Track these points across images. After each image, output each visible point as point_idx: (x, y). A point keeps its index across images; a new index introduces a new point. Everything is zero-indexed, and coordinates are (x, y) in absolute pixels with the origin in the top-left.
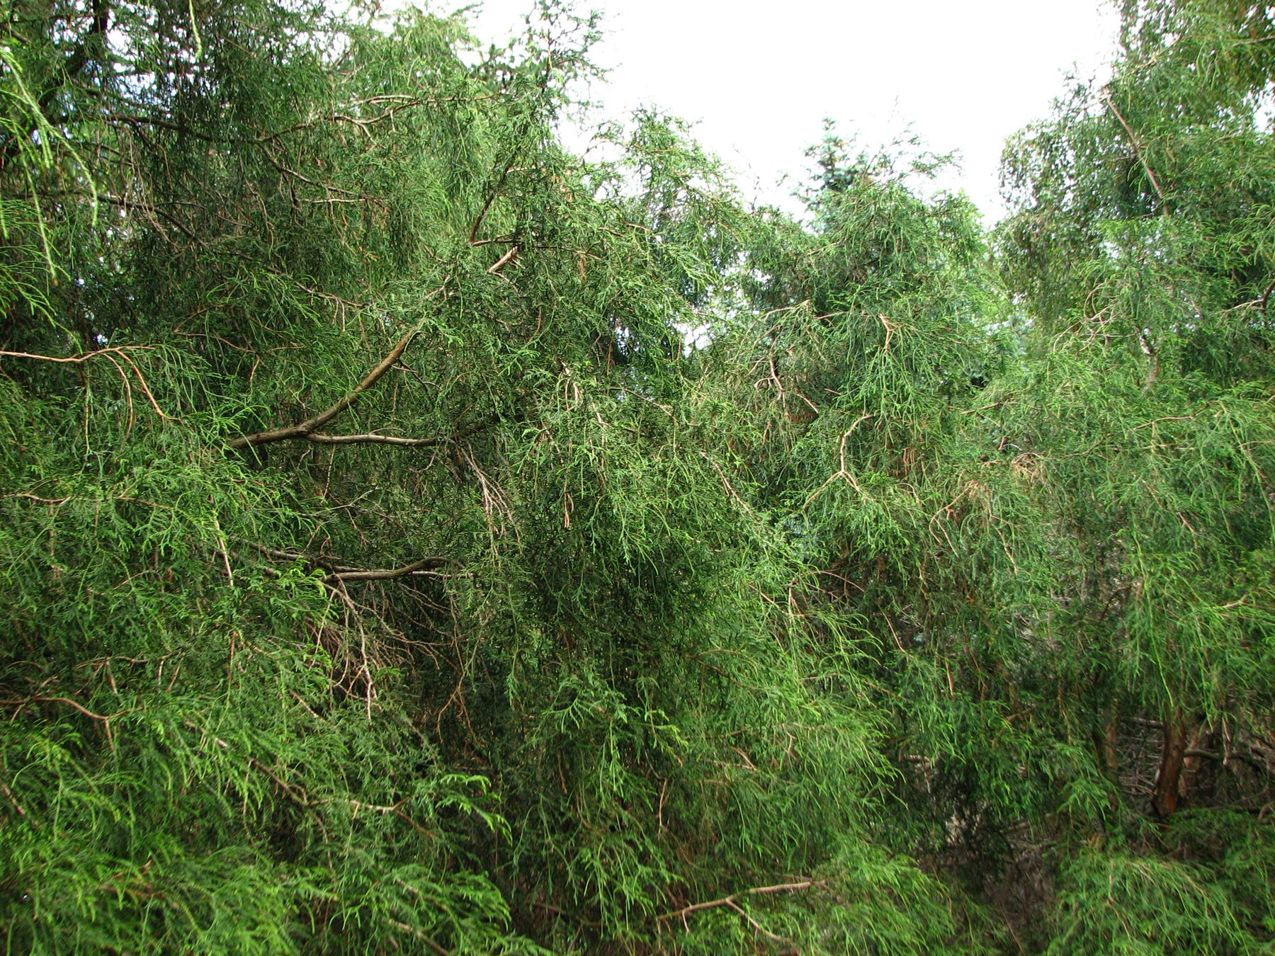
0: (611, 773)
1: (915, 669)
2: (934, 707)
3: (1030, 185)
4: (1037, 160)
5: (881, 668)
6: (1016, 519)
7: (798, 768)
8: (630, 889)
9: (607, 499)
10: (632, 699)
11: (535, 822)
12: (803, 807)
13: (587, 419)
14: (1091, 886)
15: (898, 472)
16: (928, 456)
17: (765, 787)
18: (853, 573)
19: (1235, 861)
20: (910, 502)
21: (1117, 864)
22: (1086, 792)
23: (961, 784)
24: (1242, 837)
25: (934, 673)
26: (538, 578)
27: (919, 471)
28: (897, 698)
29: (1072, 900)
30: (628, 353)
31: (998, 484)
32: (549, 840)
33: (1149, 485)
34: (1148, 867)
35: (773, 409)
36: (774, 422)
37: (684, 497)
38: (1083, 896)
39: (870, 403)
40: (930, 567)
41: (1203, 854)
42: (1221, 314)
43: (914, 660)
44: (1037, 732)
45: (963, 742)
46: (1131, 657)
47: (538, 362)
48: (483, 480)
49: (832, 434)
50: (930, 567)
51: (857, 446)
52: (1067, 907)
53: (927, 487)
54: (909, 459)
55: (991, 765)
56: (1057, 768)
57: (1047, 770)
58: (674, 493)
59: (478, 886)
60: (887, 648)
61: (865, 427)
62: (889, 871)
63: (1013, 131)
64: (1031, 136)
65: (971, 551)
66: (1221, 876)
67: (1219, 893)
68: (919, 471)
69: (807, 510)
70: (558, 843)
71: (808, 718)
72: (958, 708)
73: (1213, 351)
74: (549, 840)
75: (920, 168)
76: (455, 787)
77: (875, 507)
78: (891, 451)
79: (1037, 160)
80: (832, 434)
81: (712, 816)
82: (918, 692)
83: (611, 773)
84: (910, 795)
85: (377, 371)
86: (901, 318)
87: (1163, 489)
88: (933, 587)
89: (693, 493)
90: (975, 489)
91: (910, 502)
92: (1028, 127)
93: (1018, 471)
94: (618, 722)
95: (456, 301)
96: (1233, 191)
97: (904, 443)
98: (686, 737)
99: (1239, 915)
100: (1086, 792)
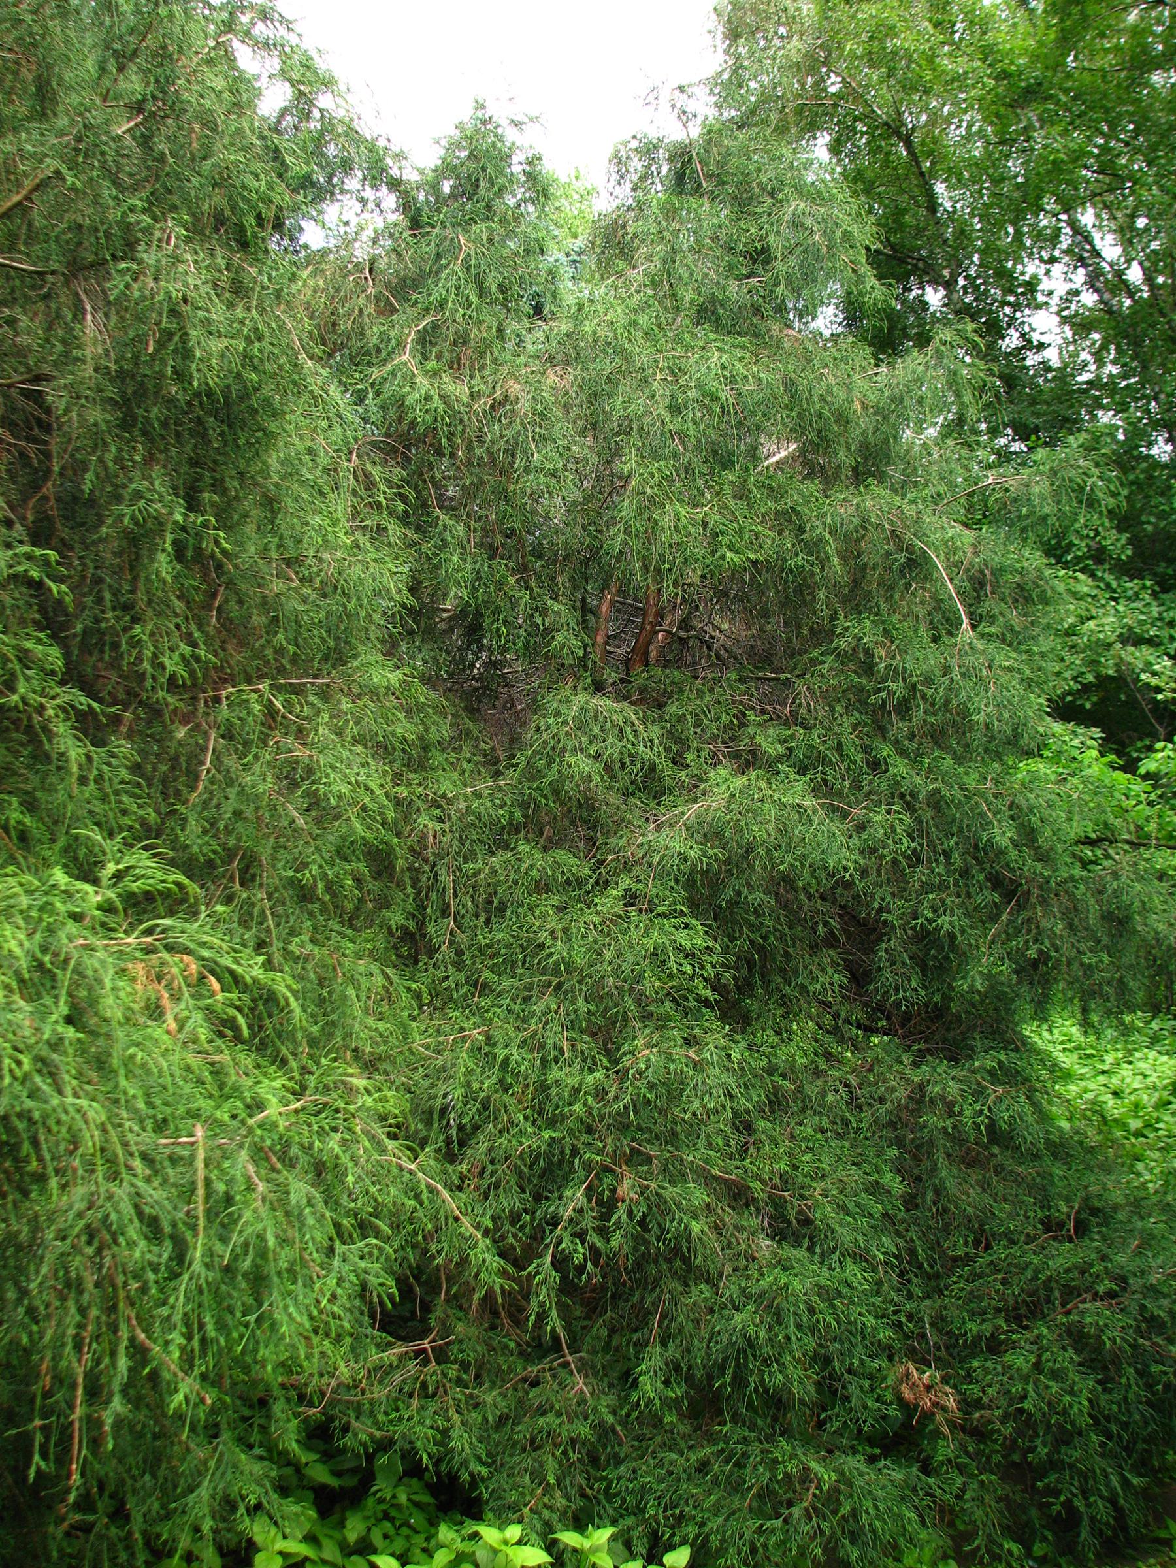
0: (163, 565)
1: (445, 526)
2: (455, 558)
3: (629, 185)
4: (636, 164)
5: (417, 518)
6: (541, 415)
7: (536, 707)
8: (171, 663)
9: (186, 334)
10: (192, 505)
11: (100, 600)
12: (334, 620)
13: (179, 269)
14: (558, 714)
15: (455, 365)
16: (482, 355)
17: (305, 600)
18: (408, 443)
19: (673, 709)
20: (458, 390)
21: (581, 698)
22: (567, 641)
23: (471, 624)
24: (681, 691)
25: (460, 530)
26: (123, 394)
27: (472, 369)
28: (427, 547)
29: (542, 723)
30: (241, 229)
31: (529, 380)
32: (110, 615)
33: (648, 404)
34: (604, 703)
35: (362, 301)
36: (361, 311)
37: (257, 344)
38: (550, 721)
39: (442, 304)
40: (470, 447)
41: (653, 702)
42: (732, 287)
43: (445, 519)
44: (536, 590)
45: (475, 589)
46: (615, 540)
47: (145, 211)
48: (88, 308)
49: (407, 327)
50: (470, 447)
51: (426, 340)
52: (538, 729)
53: (477, 380)
54: (467, 355)
55: (496, 612)
56: (547, 621)
57: (539, 621)
58: (248, 339)
59: (39, 641)
60: (425, 505)
61: (435, 326)
62: (394, 678)
63: (621, 139)
64: (634, 144)
65: (502, 437)
66: (661, 718)
67: (655, 731)
68: (472, 369)
69: (373, 384)
70: (117, 618)
71: (340, 543)
72: (475, 562)
73: (721, 312)
74: (110, 615)
75: (514, 123)
76: (29, 557)
77: (424, 386)
78: (447, 347)
79: (636, 164)
80: (407, 327)
81: (258, 619)
82: (445, 545)
83: (163, 565)
84: (418, 620)
85: (9, 204)
86: (477, 241)
87: (660, 409)
88: (469, 463)
89: (265, 343)
90: (515, 388)
91: (458, 390)
92: (634, 137)
93: (552, 378)
94: (176, 522)
95: (82, 150)
96: (757, 190)
97: (464, 343)
98: (248, 549)
99: (668, 749)
100: (567, 641)
